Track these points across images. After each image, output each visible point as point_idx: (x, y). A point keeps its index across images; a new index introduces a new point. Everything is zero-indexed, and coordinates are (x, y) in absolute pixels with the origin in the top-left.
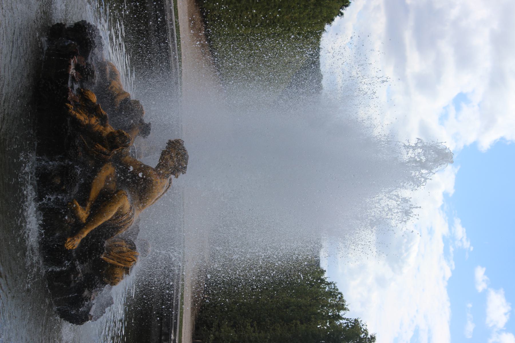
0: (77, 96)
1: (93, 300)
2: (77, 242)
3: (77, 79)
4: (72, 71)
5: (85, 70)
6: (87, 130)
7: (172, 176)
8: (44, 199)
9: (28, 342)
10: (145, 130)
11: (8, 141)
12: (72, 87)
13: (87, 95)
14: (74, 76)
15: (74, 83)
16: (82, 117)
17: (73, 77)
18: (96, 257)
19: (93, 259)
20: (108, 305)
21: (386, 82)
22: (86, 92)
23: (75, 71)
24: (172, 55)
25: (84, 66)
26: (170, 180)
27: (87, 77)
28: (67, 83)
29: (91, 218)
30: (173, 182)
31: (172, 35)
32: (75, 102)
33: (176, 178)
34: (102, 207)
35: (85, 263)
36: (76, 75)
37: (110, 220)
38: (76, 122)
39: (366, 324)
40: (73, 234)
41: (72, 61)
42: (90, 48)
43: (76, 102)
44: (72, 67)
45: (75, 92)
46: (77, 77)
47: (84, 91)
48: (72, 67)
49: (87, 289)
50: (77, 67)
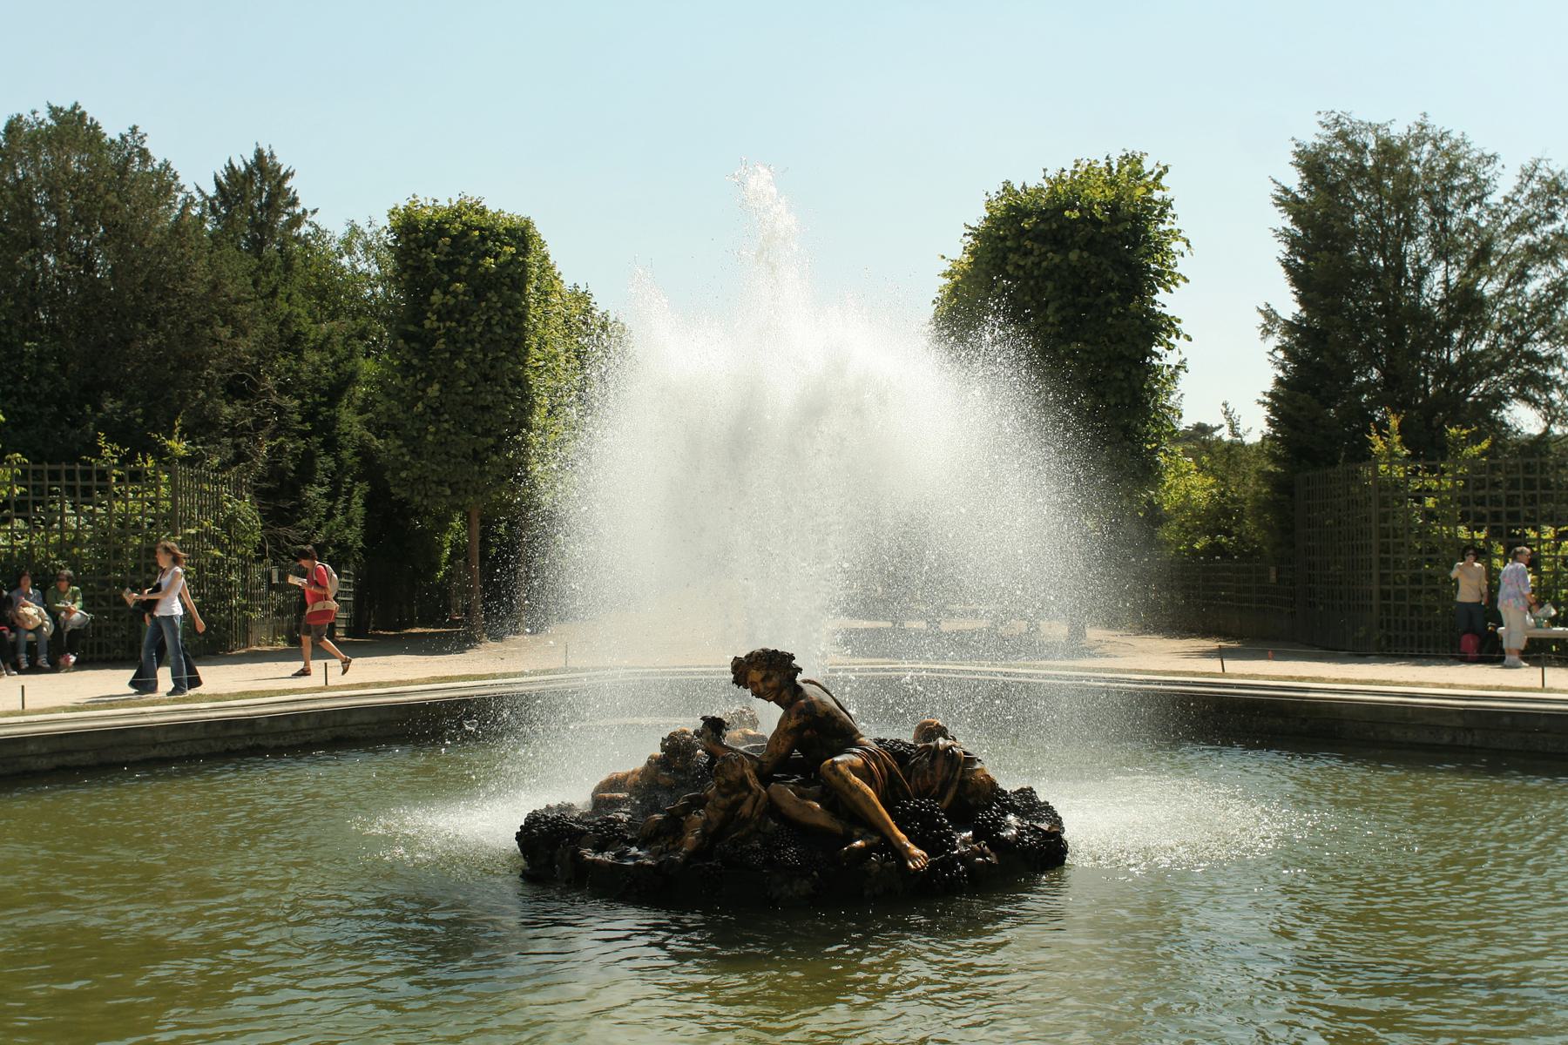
2: (917, 851)
4: (607, 857)
6: (712, 837)
7: (799, 678)
8: (1406, 452)
10: (715, 726)
11: (1531, 238)
12: (635, 857)
16: (691, 839)
21: (581, 1038)
27: (618, 831)
29: (871, 826)
30: (808, 678)
31: (547, 682)
32: (661, 853)
38: (696, 854)
39: (1163, 164)
40: (901, 855)
42: (566, 825)
50: (600, 849)
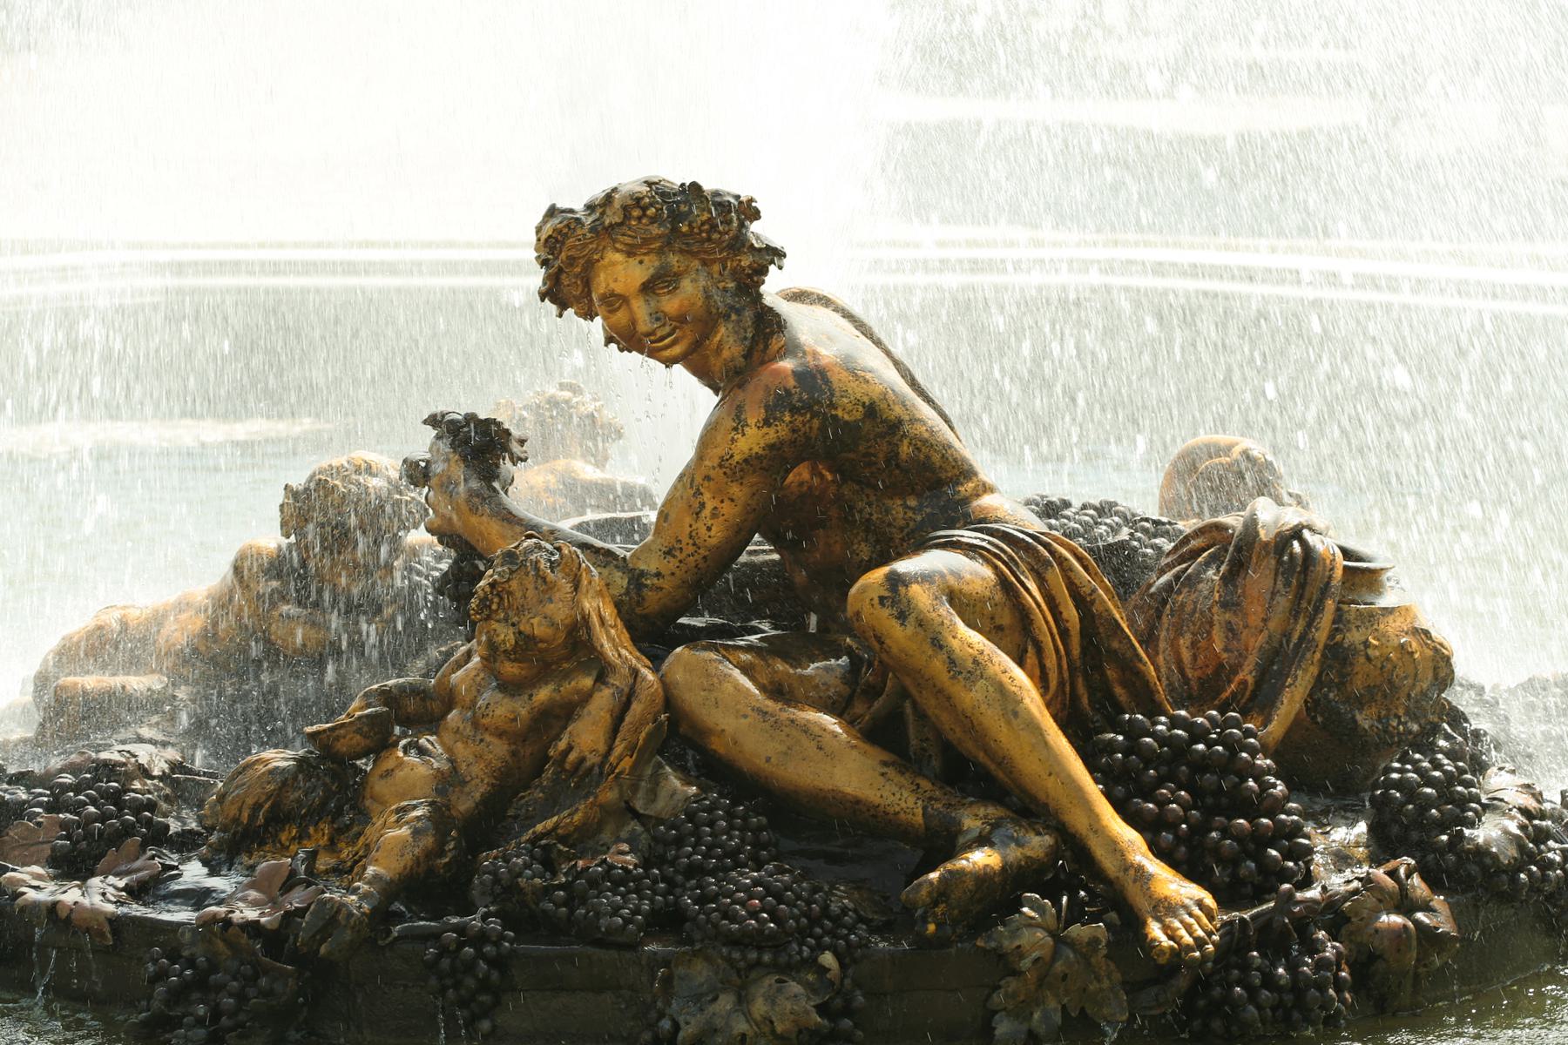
0: (252, 868)
1: (1538, 797)
3: (150, 862)
5: (92, 819)
7: (773, 287)
9: (62, 2)
12: (197, 897)
13: (245, 815)
14: (126, 889)
15: (174, 887)
17: (137, 892)
18: (1269, 771)
19: (1280, 788)
20: (1123, 584)
22: (233, 811)
23: (95, 882)
24: (1262, 638)
25: (64, 825)
26: (799, 296)
28: (180, 924)
33: (786, 262)
34: (1015, 799)
35: (1307, 837)
36: (119, 875)
37: (1042, 681)
41: (32, 895)
43: (293, 873)
44: (71, 895)
45: (222, 884)
46: (138, 863)
47: (224, 829)
48: (71, 895)
49: (1467, 832)
50: (72, 866)
